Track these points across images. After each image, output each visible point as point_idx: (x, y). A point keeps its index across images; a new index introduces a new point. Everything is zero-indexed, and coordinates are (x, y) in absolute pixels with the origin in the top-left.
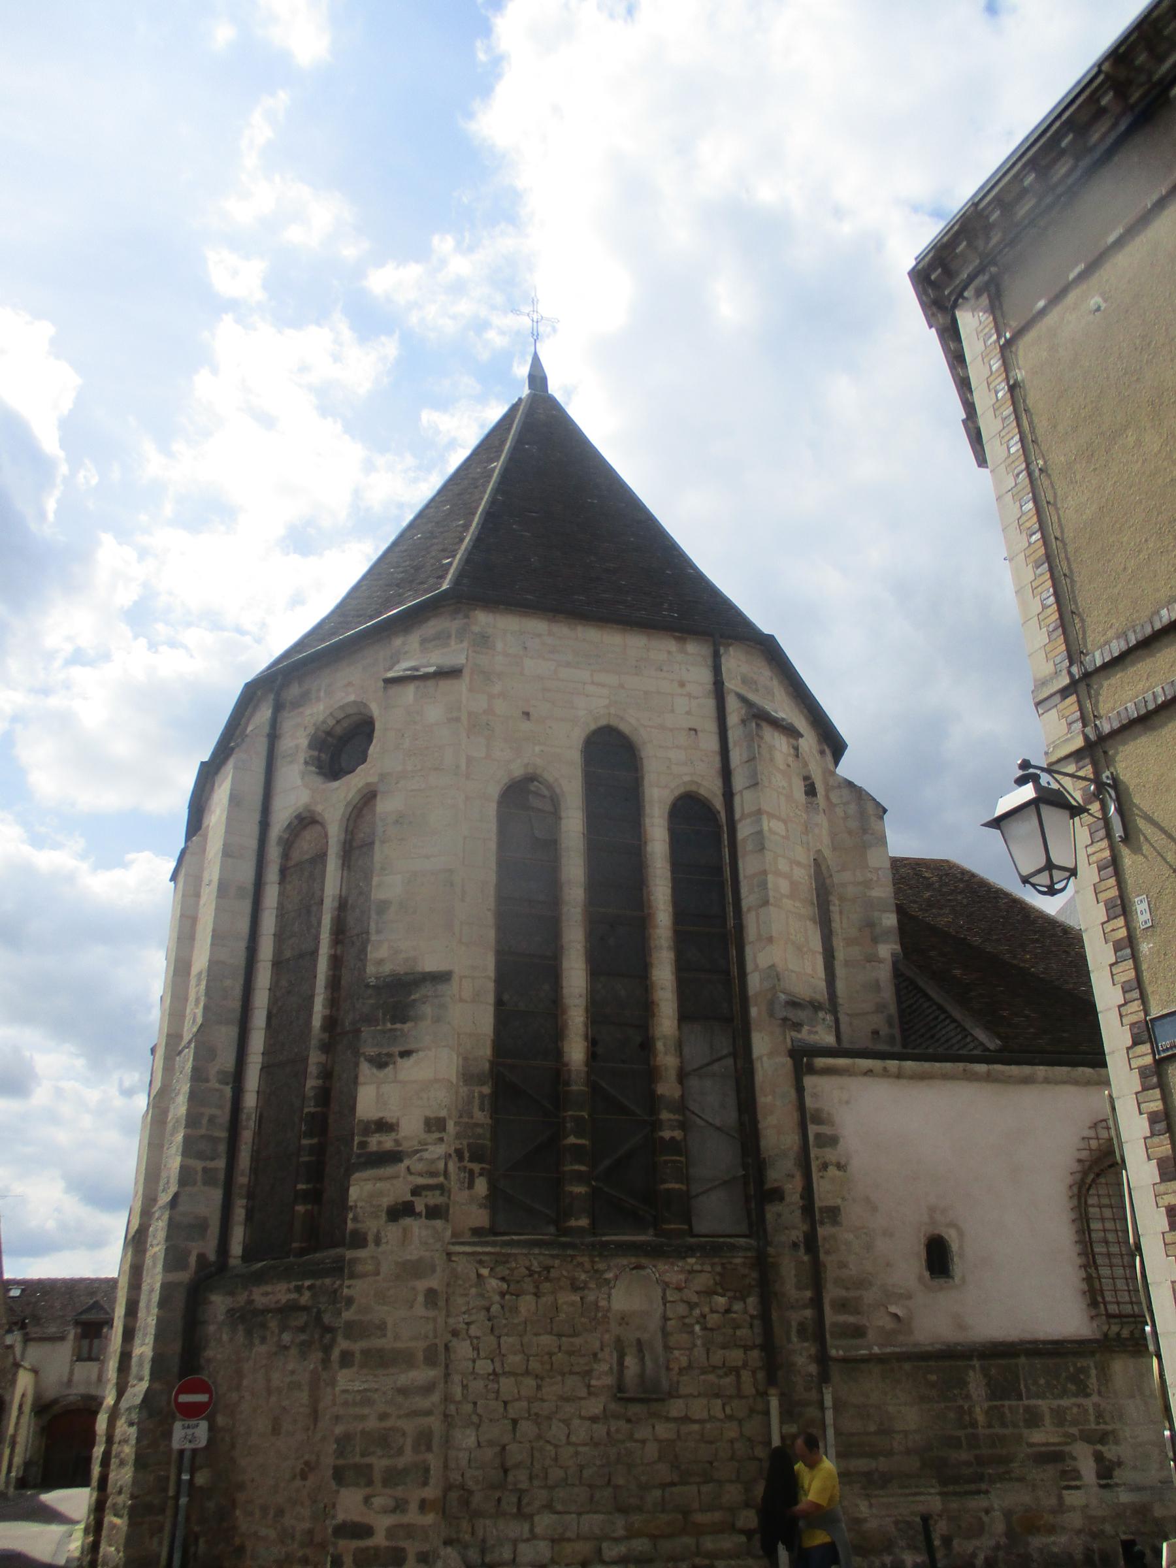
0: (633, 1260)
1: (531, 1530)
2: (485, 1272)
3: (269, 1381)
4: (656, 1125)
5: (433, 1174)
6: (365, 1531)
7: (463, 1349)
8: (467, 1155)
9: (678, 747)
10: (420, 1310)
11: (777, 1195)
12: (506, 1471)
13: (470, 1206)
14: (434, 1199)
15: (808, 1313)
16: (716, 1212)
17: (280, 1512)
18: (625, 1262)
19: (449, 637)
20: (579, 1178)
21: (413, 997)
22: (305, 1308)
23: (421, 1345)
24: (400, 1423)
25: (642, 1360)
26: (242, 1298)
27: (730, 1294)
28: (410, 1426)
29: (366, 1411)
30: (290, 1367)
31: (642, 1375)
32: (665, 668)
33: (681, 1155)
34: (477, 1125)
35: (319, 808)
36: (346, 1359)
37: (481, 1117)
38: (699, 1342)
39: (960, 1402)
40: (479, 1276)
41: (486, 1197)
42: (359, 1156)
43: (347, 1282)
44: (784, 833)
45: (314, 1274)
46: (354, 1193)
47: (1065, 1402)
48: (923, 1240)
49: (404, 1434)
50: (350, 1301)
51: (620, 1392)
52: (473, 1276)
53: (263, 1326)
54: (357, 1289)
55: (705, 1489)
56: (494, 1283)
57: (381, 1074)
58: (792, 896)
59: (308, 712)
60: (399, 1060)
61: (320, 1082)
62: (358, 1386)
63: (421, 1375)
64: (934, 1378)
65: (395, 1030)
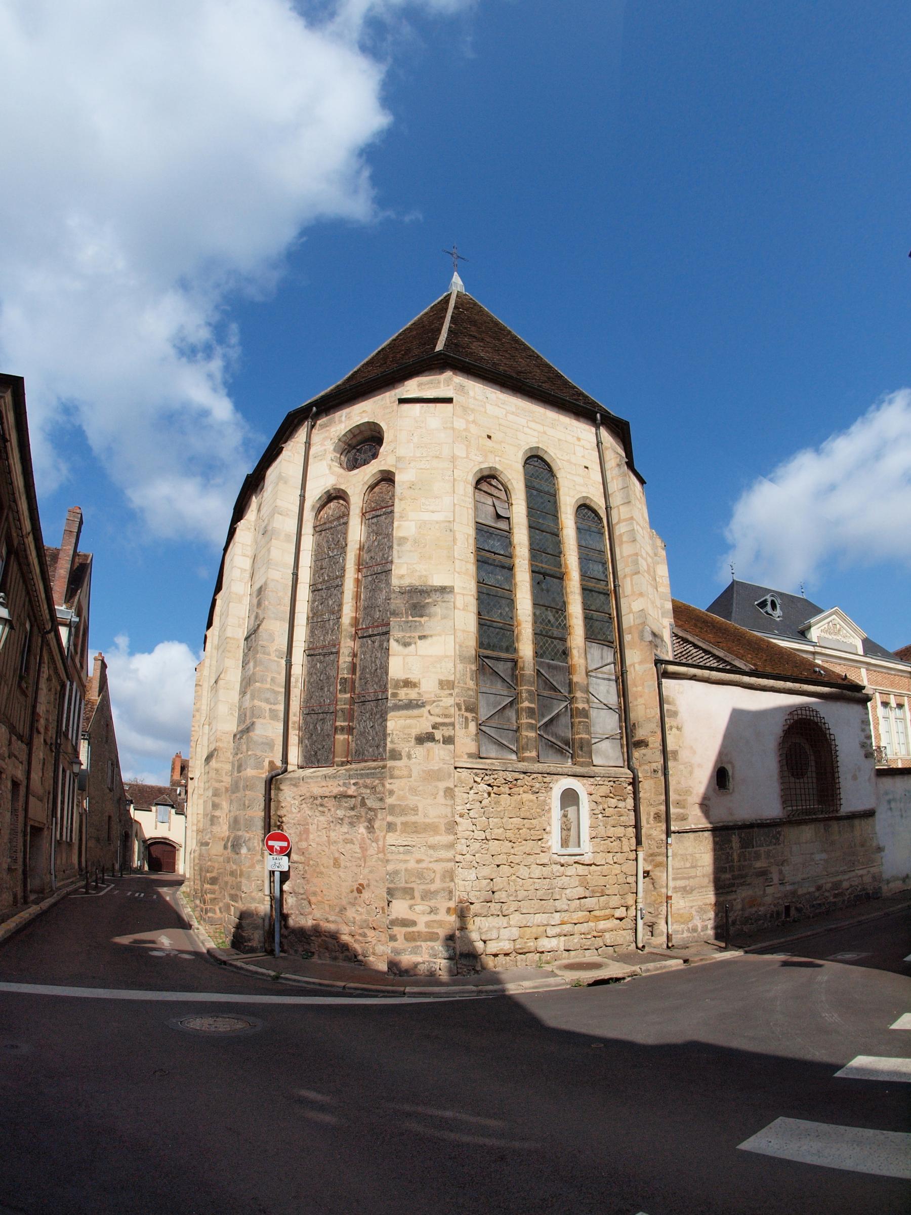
1: (508, 923)
2: (478, 779)
4: (572, 700)
6: (414, 923)
7: (464, 824)
8: (463, 708)
10: (441, 799)
12: (493, 892)
14: (448, 732)
20: (531, 727)
22: (351, 797)
23: (443, 821)
24: (431, 865)
28: (439, 867)
34: (469, 689)
36: (391, 827)
38: (601, 824)
39: (728, 850)
46: (390, 725)
47: (770, 848)
50: (391, 792)
59: (333, 429)
65: (415, 621)
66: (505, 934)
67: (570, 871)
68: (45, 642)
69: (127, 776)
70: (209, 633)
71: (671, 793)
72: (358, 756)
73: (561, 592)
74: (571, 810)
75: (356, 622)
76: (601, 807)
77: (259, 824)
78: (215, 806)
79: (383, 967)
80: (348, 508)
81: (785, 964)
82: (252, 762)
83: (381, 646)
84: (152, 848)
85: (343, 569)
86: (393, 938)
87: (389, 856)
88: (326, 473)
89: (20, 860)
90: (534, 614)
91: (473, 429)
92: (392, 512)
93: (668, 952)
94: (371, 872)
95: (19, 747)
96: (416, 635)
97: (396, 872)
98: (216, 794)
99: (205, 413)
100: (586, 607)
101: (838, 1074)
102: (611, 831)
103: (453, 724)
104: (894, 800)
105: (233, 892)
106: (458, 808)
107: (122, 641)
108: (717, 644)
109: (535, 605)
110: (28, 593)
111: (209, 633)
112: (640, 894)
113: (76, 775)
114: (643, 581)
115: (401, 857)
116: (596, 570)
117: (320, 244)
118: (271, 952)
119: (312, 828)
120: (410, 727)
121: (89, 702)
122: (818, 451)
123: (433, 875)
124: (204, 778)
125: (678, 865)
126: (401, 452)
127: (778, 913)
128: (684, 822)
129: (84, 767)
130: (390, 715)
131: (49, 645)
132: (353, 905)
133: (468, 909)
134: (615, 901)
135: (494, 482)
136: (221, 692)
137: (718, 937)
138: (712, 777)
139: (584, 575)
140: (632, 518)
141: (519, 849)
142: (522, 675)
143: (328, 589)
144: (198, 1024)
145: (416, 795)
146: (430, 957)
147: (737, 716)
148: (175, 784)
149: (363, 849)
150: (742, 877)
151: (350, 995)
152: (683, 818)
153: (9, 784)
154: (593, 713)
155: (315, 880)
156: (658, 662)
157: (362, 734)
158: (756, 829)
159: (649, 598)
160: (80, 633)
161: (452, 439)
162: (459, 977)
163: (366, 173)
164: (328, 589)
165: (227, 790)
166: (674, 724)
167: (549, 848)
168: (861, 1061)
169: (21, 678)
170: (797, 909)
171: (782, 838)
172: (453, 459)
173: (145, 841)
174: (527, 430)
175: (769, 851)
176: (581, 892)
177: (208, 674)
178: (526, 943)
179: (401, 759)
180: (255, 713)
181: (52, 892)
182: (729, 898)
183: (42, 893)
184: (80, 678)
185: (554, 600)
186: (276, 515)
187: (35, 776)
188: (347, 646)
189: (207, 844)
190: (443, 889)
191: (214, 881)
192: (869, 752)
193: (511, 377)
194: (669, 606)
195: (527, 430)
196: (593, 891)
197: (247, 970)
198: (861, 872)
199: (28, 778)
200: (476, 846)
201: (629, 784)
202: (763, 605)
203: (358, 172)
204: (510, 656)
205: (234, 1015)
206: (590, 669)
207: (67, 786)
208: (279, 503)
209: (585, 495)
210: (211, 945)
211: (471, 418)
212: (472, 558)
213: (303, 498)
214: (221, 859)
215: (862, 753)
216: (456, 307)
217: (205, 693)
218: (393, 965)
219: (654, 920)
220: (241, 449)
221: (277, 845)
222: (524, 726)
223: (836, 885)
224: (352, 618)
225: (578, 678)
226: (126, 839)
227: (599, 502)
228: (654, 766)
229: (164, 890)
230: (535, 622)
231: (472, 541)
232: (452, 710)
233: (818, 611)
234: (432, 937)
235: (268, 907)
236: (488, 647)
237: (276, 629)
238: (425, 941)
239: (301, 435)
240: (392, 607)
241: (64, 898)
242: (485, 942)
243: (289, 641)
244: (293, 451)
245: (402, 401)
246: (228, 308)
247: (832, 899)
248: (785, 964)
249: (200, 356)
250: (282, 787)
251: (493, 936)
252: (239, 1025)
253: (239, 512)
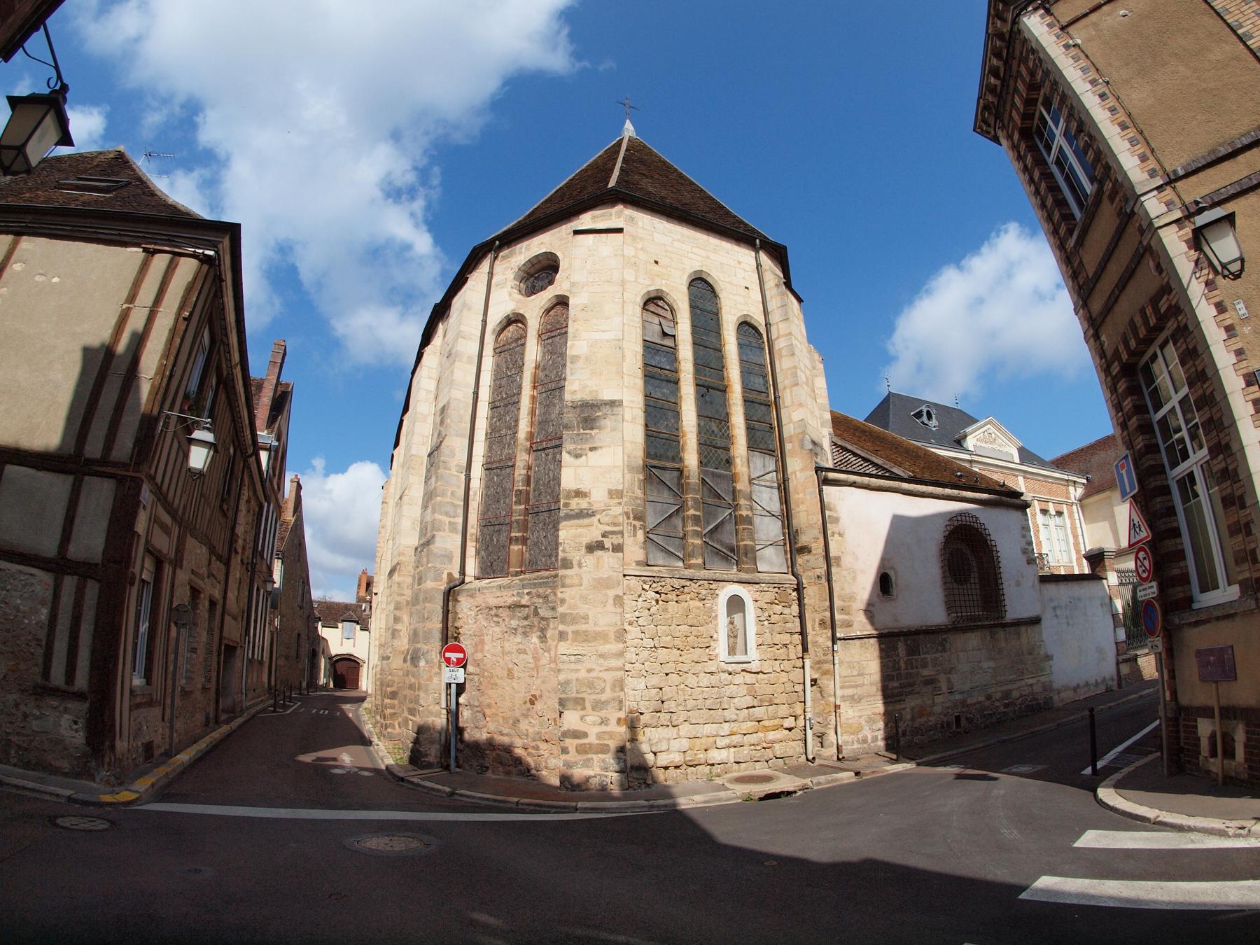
2: (647, 587)
4: (736, 507)
6: (585, 735)
7: (634, 632)
10: (610, 606)
11: (805, 550)
13: (634, 548)
14: (616, 540)
20: (697, 534)
22: (525, 606)
23: (613, 629)
24: (601, 675)
28: (609, 677)
36: (562, 636)
46: (563, 534)
47: (937, 655)
50: (563, 601)
66: (675, 745)
67: (738, 679)
68: (247, 466)
69: (316, 594)
70: (395, 453)
71: (835, 599)
72: (530, 566)
73: (725, 404)
74: (737, 617)
75: (531, 436)
76: (766, 614)
77: (437, 635)
78: (397, 620)
79: (556, 781)
80: (525, 330)
81: (959, 777)
82: (431, 574)
83: (554, 458)
84: (339, 665)
85: (520, 387)
86: (565, 751)
87: (561, 666)
88: (506, 300)
89: (214, 679)
90: (699, 425)
91: (642, 255)
92: (566, 333)
93: (839, 764)
94: (543, 682)
95: (218, 566)
96: (587, 446)
97: (568, 682)
98: (397, 608)
99: (407, 247)
100: (748, 418)
101: (1023, 896)
102: (777, 639)
103: (621, 533)
104: (1059, 607)
105: (411, 706)
107: (319, 463)
108: (875, 452)
109: (699, 416)
110: (233, 420)
111: (395, 453)
112: (809, 703)
113: (269, 593)
114: (802, 393)
115: (573, 666)
116: (757, 382)
117: (522, 93)
118: (447, 768)
119: (487, 639)
120: (580, 536)
121: (284, 522)
122: (960, 268)
124: (387, 592)
125: (845, 673)
126: (576, 277)
127: (948, 724)
129: (276, 586)
130: (562, 525)
131: (249, 468)
132: (526, 716)
133: (638, 719)
134: (783, 710)
135: (661, 303)
136: (405, 507)
137: (889, 748)
138: (875, 583)
139: (746, 388)
140: (790, 334)
141: (687, 657)
143: (505, 406)
144: (375, 843)
146: (600, 770)
147: (899, 524)
148: (361, 600)
149: (536, 659)
150: (911, 685)
151: (523, 812)
152: (849, 625)
153: (207, 603)
154: (757, 520)
155: (490, 692)
156: (818, 469)
157: (536, 544)
158: (921, 637)
159: (808, 408)
160: (279, 457)
161: (621, 264)
162: (631, 791)
163: (565, 32)
164: (505, 406)
165: (408, 603)
166: (836, 530)
167: (717, 656)
168: (1046, 882)
169: (222, 501)
170: (967, 719)
171: (948, 646)
172: (623, 283)
173: (331, 658)
174: (691, 255)
175: (936, 659)
176: (749, 701)
177: (394, 491)
180: (436, 526)
181: (242, 711)
182: (898, 707)
183: (233, 712)
184: (277, 500)
185: (717, 411)
186: (460, 340)
187: (231, 595)
188: (522, 459)
189: (388, 658)
191: (394, 695)
192: (1031, 558)
193: (677, 209)
194: (828, 416)
195: (691, 255)
196: (761, 700)
197: (424, 787)
198: (1031, 681)
199: (225, 598)
200: (645, 654)
202: (919, 415)
203: (558, 32)
204: (677, 466)
205: (409, 834)
207: (261, 601)
208: (463, 328)
210: (390, 761)
211: (640, 246)
212: (639, 373)
213: (484, 322)
214: (401, 673)
215: (1024, 559)
216: (627, 150)
217: (390, 510)
218: (565, 779)
219: (823, 730)
220: (439, 279)
221: (454, 656)
223: (1007, 694)
225: (742, 486)
226: (314, 656)
227: (759, 320)
228: (818, 572)
229: (347, 707)
230: (699, 433)
231: (640, 357)
232: (621, 519)
233: (973, 421)
234: (603, 749)
235: (445, 721)
236: (656, 457)
237: (456, 445)
238: (597, 753)
239: (485, 266)
240: (565, 421)
241: (254, 716)
242: (655, 754)
243: (467, 455)
244: (477, 281)
245: (577, 232)
246: (435, 153)
247: (1002, 709)
248: (959, 777)
249: (404, 197)
250: (460, 598)
251: (664, 747)
252: (415, 844)
253: (427, 338)
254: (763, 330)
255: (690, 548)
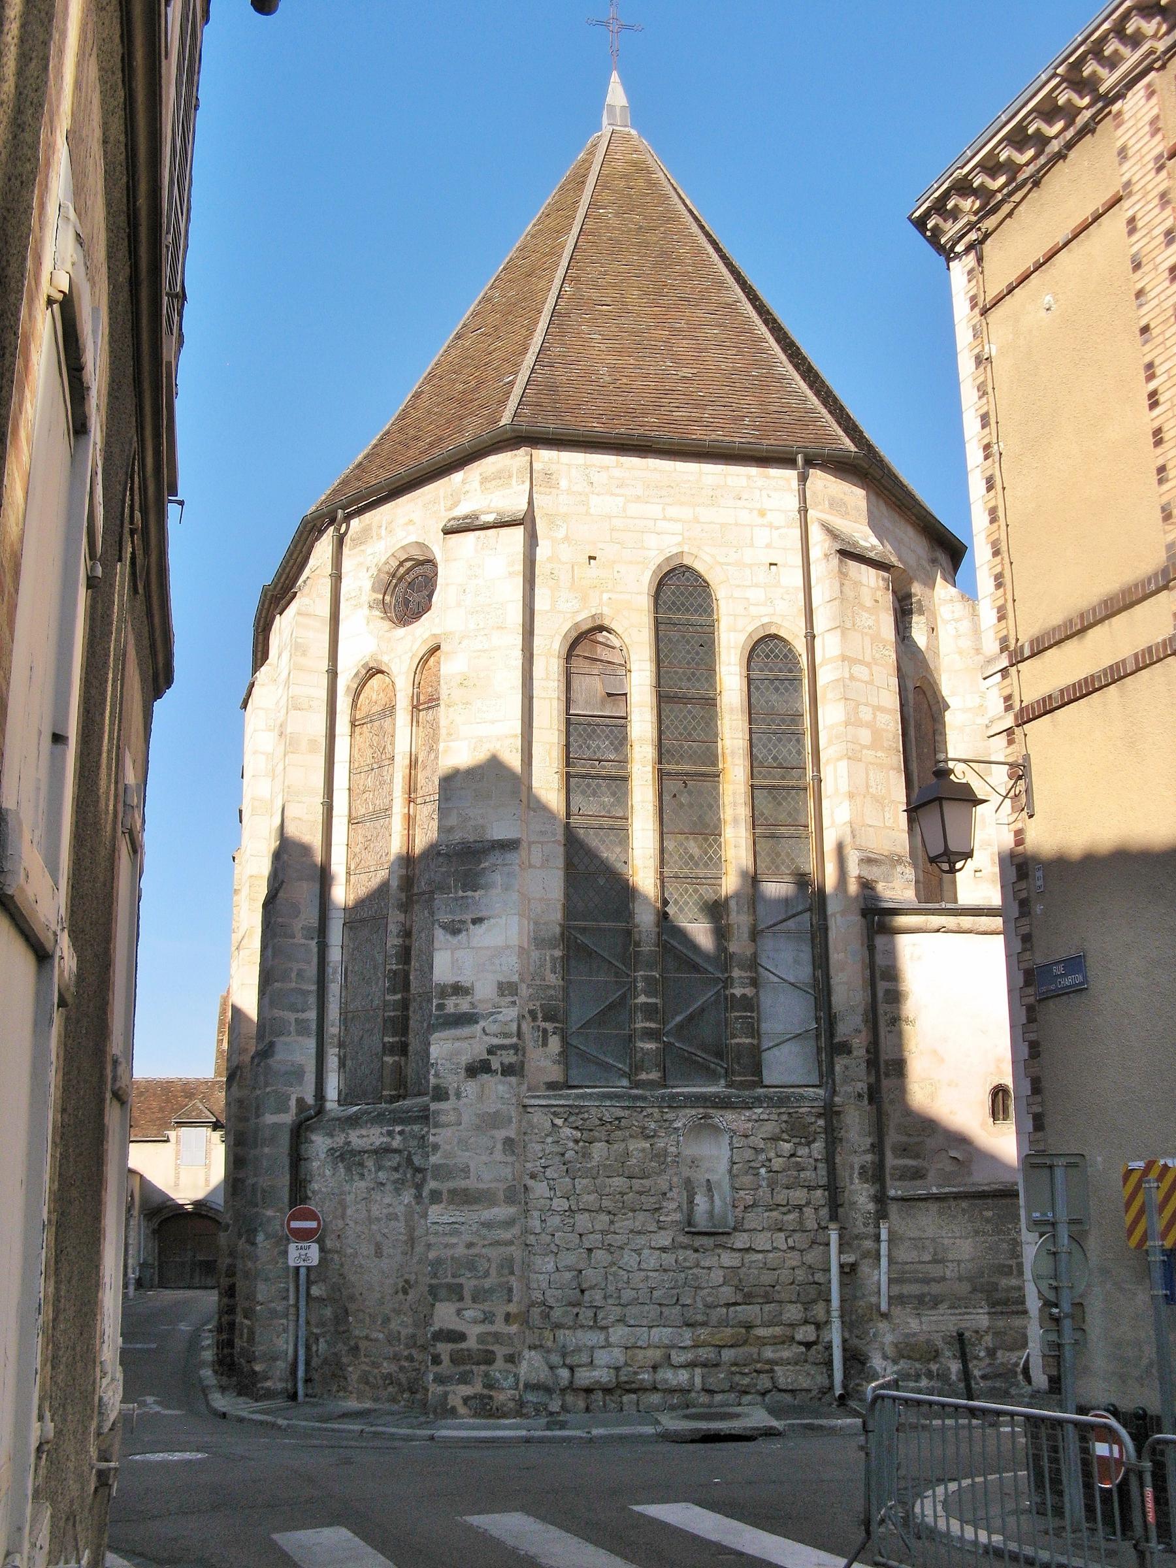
0: (701, 1110)
1: (607, 1340)
2: (559, 1122)
3: (369, 1211)
4: (728, 982)
5: (506, 1035)
6: (462, 1337)
7: (540, 1189)
8: (540, 1015)
9: (757, 586)
10: (498, 1156)
11: (845, 1048)
12: (582, 1291)
13: (544, 1061)
14: (509, 1058)
15: (869, 1157)
16: (787, 1065)
17: (387, 1320)
18: (693, 1112)
19: (510, 477)
20: (650, 1035)
21: (482, 866)
22: (396, 1151)
23: (502, 1186)
25: (712, 1198)
26: (340, 1140)
27: (797, 1140)
29: (454, 1240)
30: (387, 1200)
31: (711, 1213)
32: (745, 497)
33: (752, 1012)
34: (549, 987)
35: (385, 659)
36: (436, 1197)
37: (553, 979)
38: (764, 1184)
40: (554, 1125)
41: (560, 1054)
42: (439, 1017)
43: (433, 1131)
44: (866, 678)
45: (401, 1121)
46: (435, 1051)
48: (989, 1088)
49: (489, 1260)
50: (436, 1147)
51: (689, 1227)
52: (548, 1125)
53: (361, 1164)
54: (440, 1136)
55: (767, 1308)
56: (568, 1131)
57: (454, 940)
58: (875, 745)
60: (471, 926)
61: (401, 940)
62: (445, 1219)
63: (502, 1212)
64: (990, 1214)
97: (439, 1262)
106: (529, 1165)
119: (349, 1198)
123: (486, 1265)
128: (918, 1183)
141: (625, 1223)
142: (637, 953)
145: (467, 1150)
176: (727, 1293)
178: (636, 1373)
179: (448, 1099)
190: (500, 1285)
201: (819, 1116)
206: (761, 927)
209: (765, 620)
213: (333, 673)
222: (638, 1033)
224: (401, 877)
238: (478, 1364)
242: (572, 1369)
254: (800, 646)
255: (639, 1055)
